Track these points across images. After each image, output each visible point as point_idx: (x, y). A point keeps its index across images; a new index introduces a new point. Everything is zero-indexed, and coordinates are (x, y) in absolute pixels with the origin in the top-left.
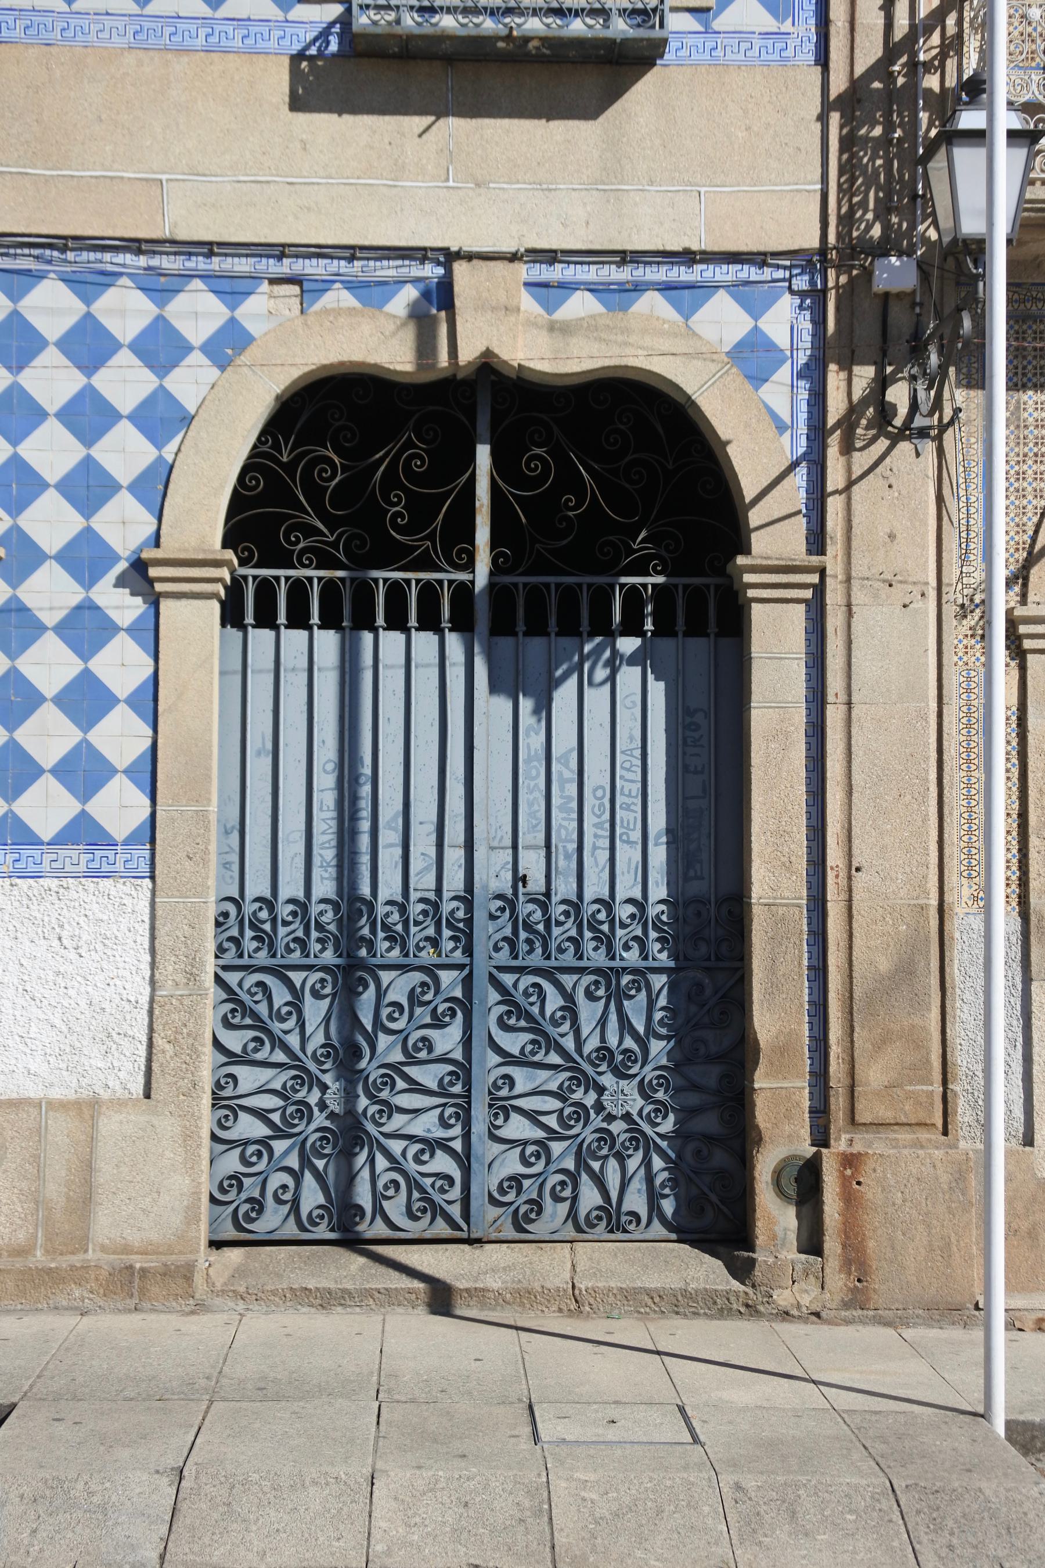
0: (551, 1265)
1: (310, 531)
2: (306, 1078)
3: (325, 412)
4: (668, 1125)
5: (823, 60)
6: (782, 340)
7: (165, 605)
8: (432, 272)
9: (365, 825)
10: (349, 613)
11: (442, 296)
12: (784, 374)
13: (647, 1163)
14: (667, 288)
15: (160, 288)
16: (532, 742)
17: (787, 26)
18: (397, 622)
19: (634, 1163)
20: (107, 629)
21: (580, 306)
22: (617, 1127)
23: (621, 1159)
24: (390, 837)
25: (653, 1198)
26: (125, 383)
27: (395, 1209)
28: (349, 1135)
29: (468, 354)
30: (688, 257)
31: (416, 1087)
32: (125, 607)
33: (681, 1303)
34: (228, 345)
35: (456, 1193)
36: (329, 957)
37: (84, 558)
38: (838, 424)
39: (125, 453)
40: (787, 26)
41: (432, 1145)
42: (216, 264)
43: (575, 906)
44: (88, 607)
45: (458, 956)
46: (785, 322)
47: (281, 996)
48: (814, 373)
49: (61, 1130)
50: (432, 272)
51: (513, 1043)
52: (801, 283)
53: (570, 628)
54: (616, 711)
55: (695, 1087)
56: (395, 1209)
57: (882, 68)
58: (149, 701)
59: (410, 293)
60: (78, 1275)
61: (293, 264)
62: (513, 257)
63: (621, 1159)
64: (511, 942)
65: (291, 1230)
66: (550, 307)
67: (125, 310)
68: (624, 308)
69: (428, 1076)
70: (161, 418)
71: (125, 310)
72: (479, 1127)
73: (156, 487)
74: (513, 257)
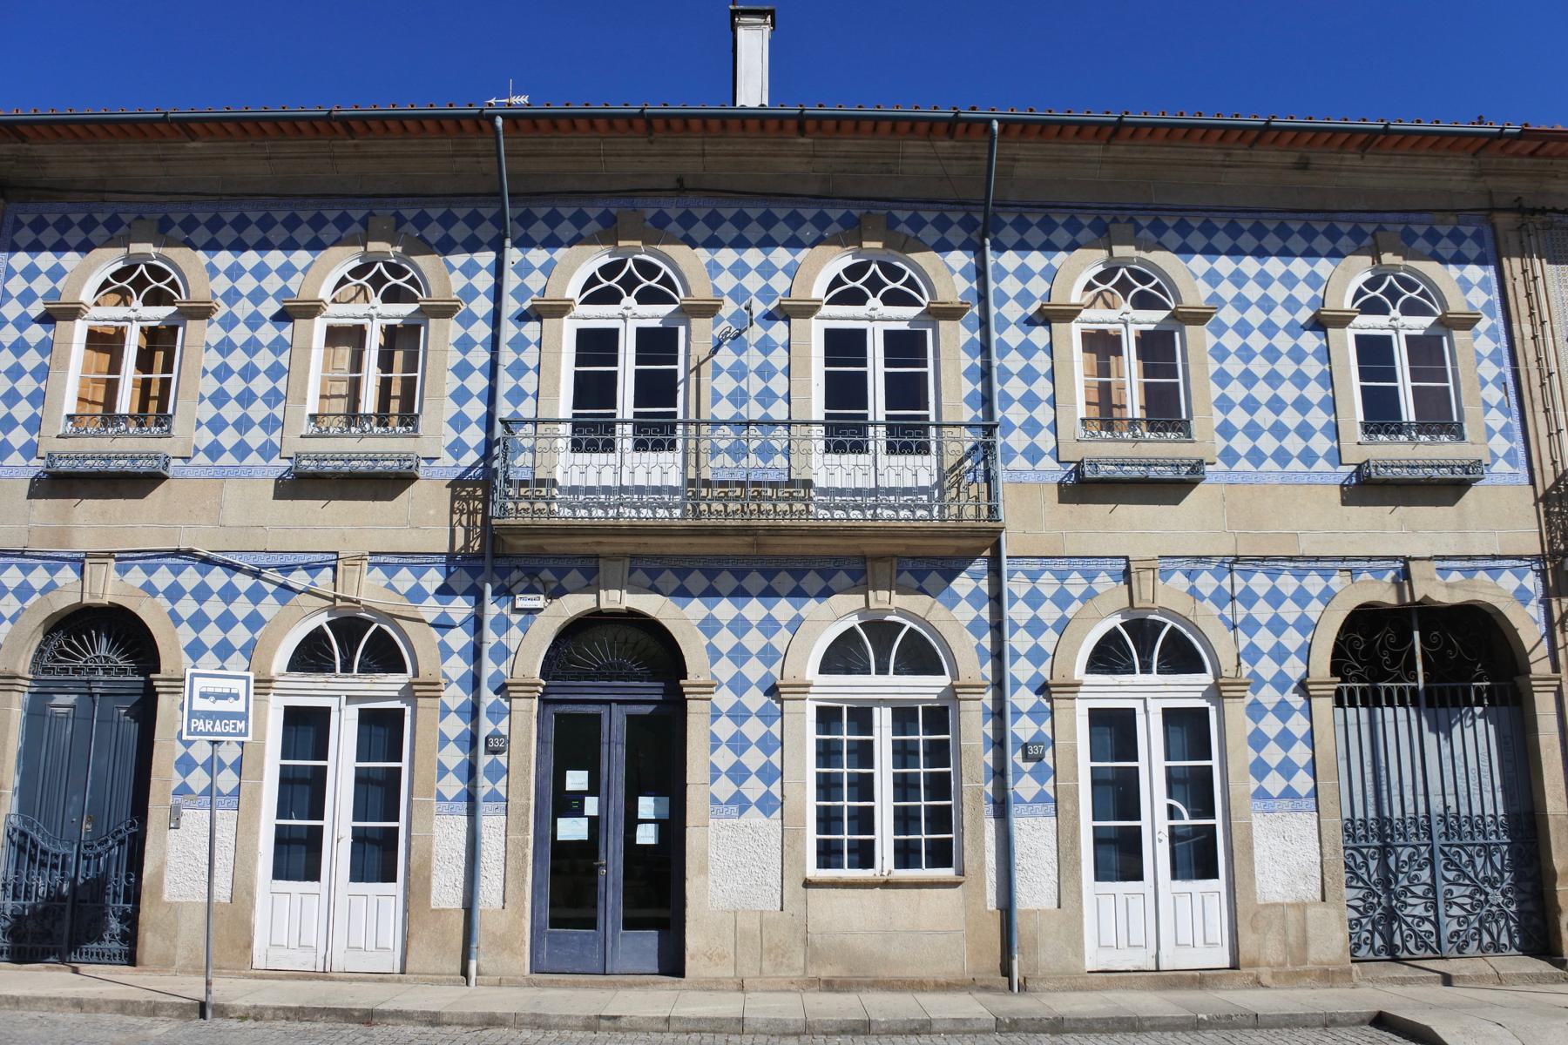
0: (1482, 966)
1: (1354, 668)
2: (1373, 894)
3: (1363, 621)
4: (1513, 908)
5: (1532, 482)
6: (1532, 589)
7: (1314, 701)
8: (1399, 565)
9: (1385, 788)
10: (1371, 700)
11: (1405, 574)
12: (1534, 602)
13: (1507, 923)
14: (1486, 569)
15: (1300, 575)
16: (1446, 751)
18: (1390, 704)
19: (1502, 923)
20: (1291, 710)
21: (1455, 577)
22: (1494, 909)
23: (1497, 922)
24: (1395, 792)
25: (1511, 937)
26: (1290, 611)
27: (1411, 945)
28: (1391, 915)
29: (1418, 598)
30: (1494, 557)
31: (1415, 896)
32: (1297, 701)
33: (1539, 979)
34: (1327, 596)
35: (1433, 939)
36: (1376, 842)
37: (1280, 682)
39: (1292, 639)
41: (1423, 919)
42: (1319, 564)
43: (1470, 818)
44: (1283, 702)
45: (1426, 841)
46: (1532, 582)
47: (1359, 859)
48: (1546, 603)
49: (1292, 915)
50: (1399, 565)
51: (1451, 875)
52: (1536, 567)
53: (1456, 705)
54: (1476, 737)
55: (1523, 892)
56: (1411, 945)
57: (1555, 485)
59: (1392, 574)
60: (1307, 974)
61: (1349, 564)
62: (1430, 559)
63: (1497, 922)
64: (1446, 834)
65: (1371, 956)
66: (1444, 578)
67: (1287, 583)
68: (1471, 577)
69: (1419, 890)
70: (1305, 626)
71: (1287, 583)
72: (1441, 911)
73: (1306, 652)
74: (1430, 559)
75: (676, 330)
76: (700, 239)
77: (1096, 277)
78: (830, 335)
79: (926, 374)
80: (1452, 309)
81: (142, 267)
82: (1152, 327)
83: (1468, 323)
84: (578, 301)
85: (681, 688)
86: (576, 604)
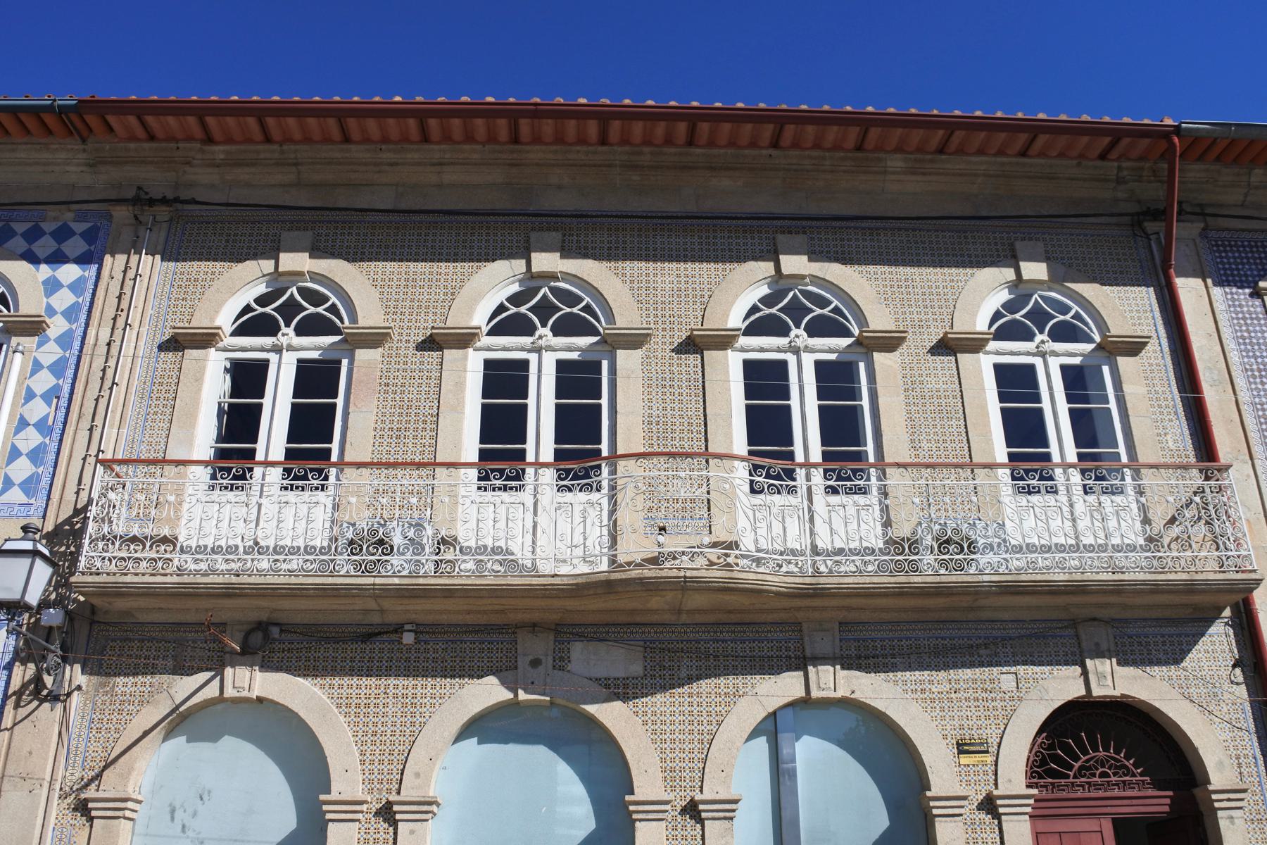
17: (32, 501)
38: (14, 693)
40: (32, 501)
58: (882, 640)
75: (600, 363)
76: (41, 253)
77: (256, 301)
78: (749, 366)
79: (600, 405)
80: (1113, 332)
81: (294, 289)
82: (833, 357)
83: (1134, 348)
84: (485, 329)
85: (626, 805)
86: (1059, 685)
